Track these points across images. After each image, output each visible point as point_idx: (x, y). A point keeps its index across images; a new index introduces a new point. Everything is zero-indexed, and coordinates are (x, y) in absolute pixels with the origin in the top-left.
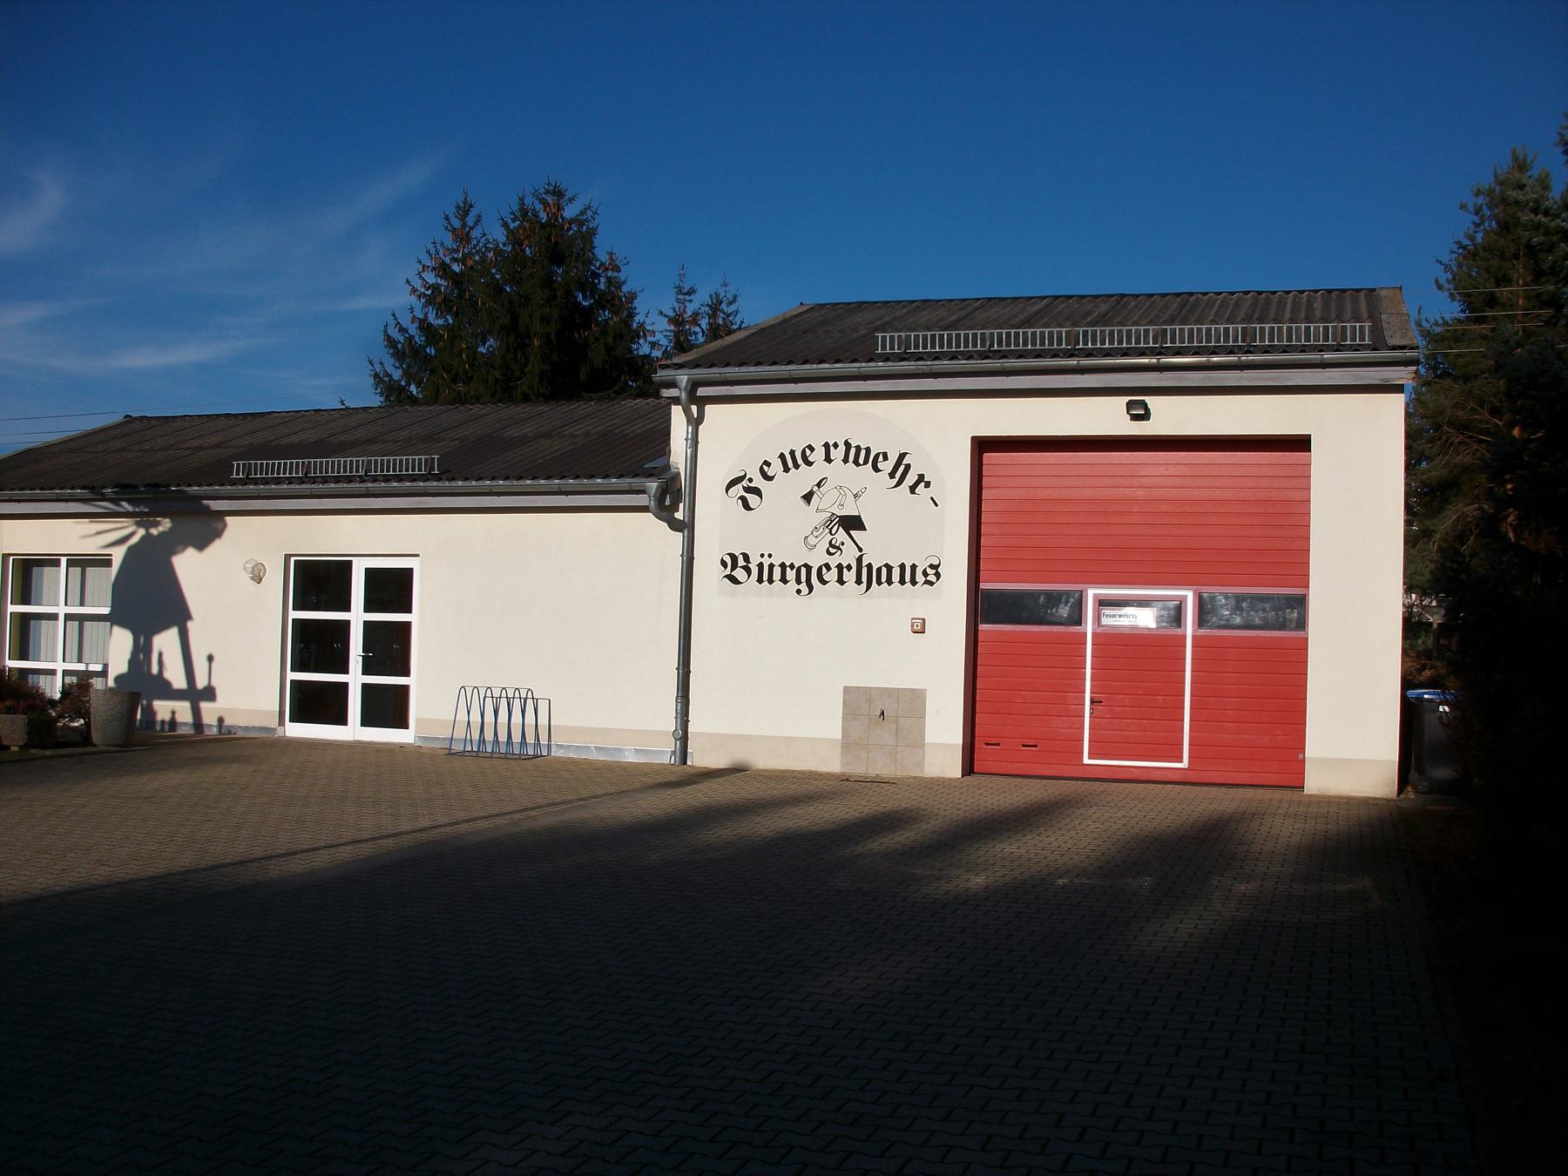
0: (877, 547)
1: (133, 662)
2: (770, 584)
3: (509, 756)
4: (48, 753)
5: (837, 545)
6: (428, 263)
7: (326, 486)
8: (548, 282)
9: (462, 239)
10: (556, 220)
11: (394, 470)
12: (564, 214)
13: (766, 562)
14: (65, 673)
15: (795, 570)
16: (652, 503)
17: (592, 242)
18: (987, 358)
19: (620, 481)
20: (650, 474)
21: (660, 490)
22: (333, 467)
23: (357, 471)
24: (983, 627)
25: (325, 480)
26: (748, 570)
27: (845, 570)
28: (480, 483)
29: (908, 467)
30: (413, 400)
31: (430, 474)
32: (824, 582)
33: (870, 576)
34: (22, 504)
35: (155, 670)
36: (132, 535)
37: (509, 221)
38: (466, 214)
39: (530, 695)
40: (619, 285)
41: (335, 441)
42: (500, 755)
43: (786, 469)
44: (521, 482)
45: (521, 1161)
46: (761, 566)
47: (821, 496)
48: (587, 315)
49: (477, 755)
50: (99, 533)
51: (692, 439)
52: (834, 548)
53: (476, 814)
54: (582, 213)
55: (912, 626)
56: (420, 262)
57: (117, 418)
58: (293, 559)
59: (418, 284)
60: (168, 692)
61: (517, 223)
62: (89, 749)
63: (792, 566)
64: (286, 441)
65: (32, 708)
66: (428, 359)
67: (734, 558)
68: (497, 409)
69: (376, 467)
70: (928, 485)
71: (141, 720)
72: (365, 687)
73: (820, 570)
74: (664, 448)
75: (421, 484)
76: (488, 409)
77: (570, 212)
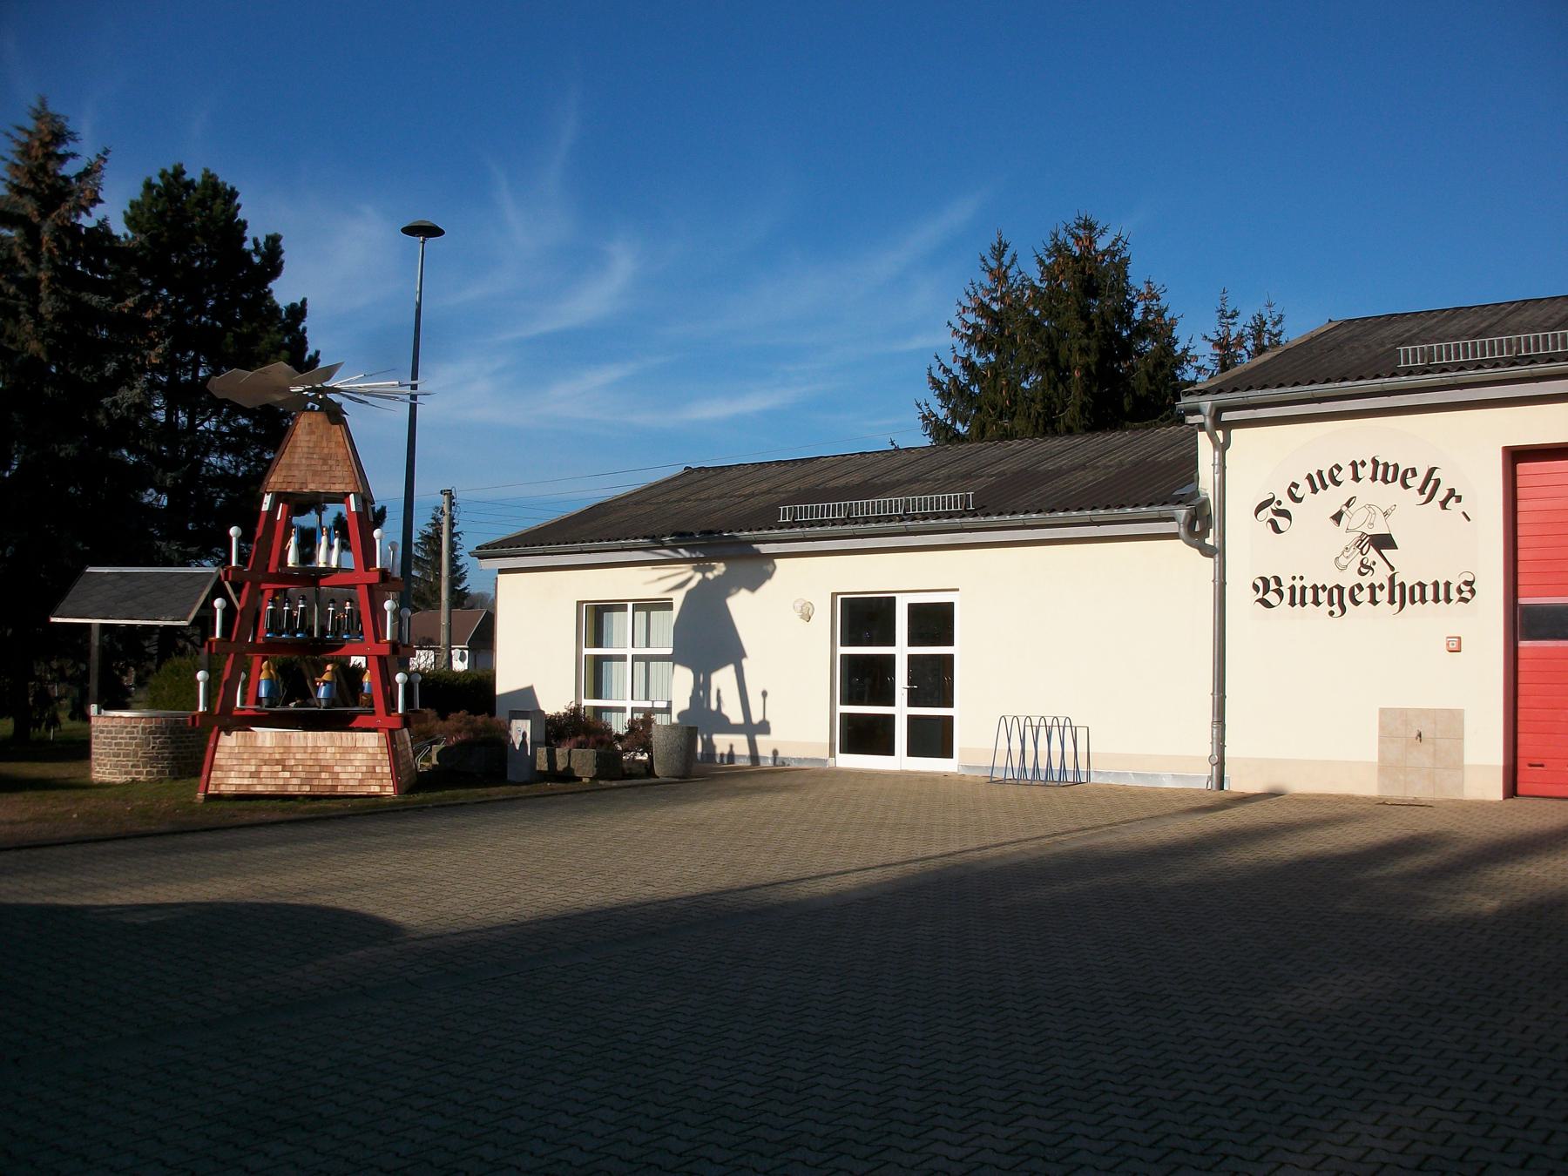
0: (1409, 565)
1: (694, 699)
2: (1303, 606)
3: (1020, 782)
4: (614, 784)
5: (1368, 564)
6: (967, 303)
7: (868, 526)
8: (1084, 315)
9: (999, 279)
10: (1089, 252)
11: (932, 508)
12: (1097, 247)
13: (1298, 584)
14: (634, 710)
15: (1327, 592)
16: (1182, 529)
17: (1126, 272)
18: (1514, 364)
19: (1149, 509)
20: (1179, 501)
21: (1189, 517)
22: (873, 508)
23: (897, 510)
24: (1523, 644)
25: (866, 521)
26: (1280, 594)
27: (1377, 590)
28: (1014, 517)
29: (1438, 482)
30: (959, 438)
31: (848, 517)
32: (1356, 603)
33: (1403, 595)
34: (592, 555)
35: (714, 706)
36: (690, 579)
37: (1044, 258)
38: (1002, 254)
39: (1068, 723)
40: (1160, 314)
41: (878, 482)
42: (1053, 784)
43: (1315, 490)
44: (1053, 515)
45: (967, 1157)
46: (1292, 588)
47: (1350, 516)
48: (1126, 350)
49: (1016, 782)
50: (660, 579)
51: (1219, 464)
52: (1365, 568)
53: (1006, 840)
54: (1114, 244)
55: (1448, 645)
56: (960, 304)
57: (680, 470)
58: (839, 597)
59: (957, 324)
60: (726, 727)
61: (1053, 259)
62: (653, 780)
63: (1324, 588)
64: (832, 484)
65: (601, 742)
66: (971, 396)
67: (1265, 581)
68: (1034, 443)
69: (914, 506)
70: (1459, 499)
71: (702, 754)
72: (911, 719)
73: (1352, 591)
74: (1192, 476)
75: (957, 520)
76: (1026, 444)
77: (1102, 244)
